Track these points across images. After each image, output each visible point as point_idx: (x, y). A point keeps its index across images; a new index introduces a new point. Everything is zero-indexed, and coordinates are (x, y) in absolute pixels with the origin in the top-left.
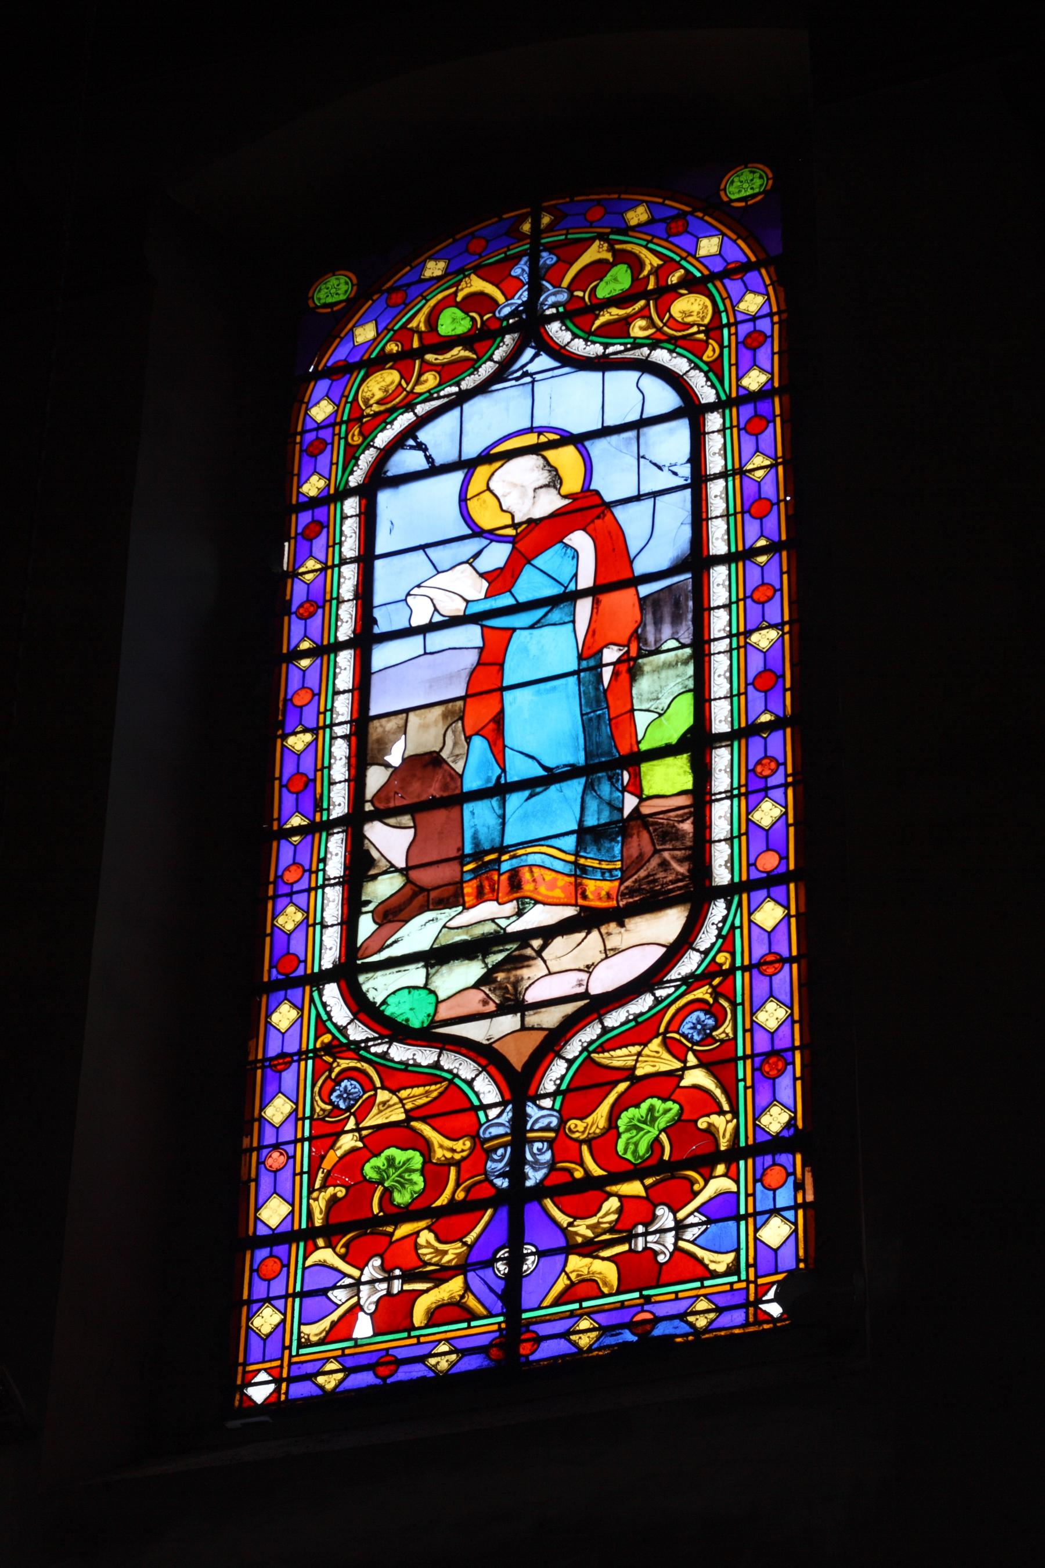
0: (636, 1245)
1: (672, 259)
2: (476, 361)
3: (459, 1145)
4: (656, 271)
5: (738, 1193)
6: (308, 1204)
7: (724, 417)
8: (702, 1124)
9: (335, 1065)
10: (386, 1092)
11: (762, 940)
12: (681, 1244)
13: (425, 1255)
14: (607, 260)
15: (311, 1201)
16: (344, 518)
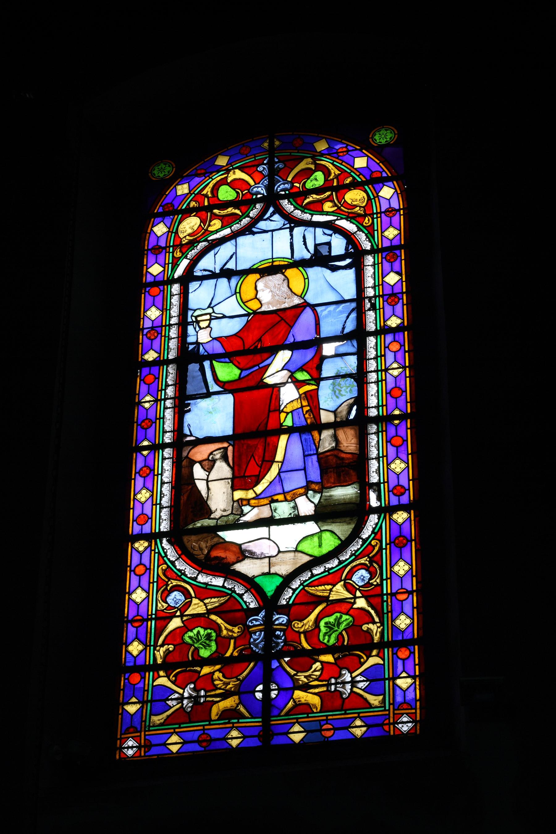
0: (331, 689)
1: (346, 171)
2: (241, 216)
3: (236, 629)
4: (337, 177)
5: (384, 664)
6: (154, 654)
7: (374, 259)
8: (365, 627)
9: (170, 583)
10: (197, 600)
11: (195, 391)
12: (355, 689)
13: (218, 685)
14: (311, 169)
15: (156, 652)
16: (172, 295)
